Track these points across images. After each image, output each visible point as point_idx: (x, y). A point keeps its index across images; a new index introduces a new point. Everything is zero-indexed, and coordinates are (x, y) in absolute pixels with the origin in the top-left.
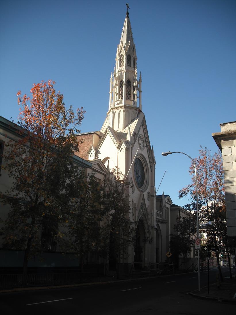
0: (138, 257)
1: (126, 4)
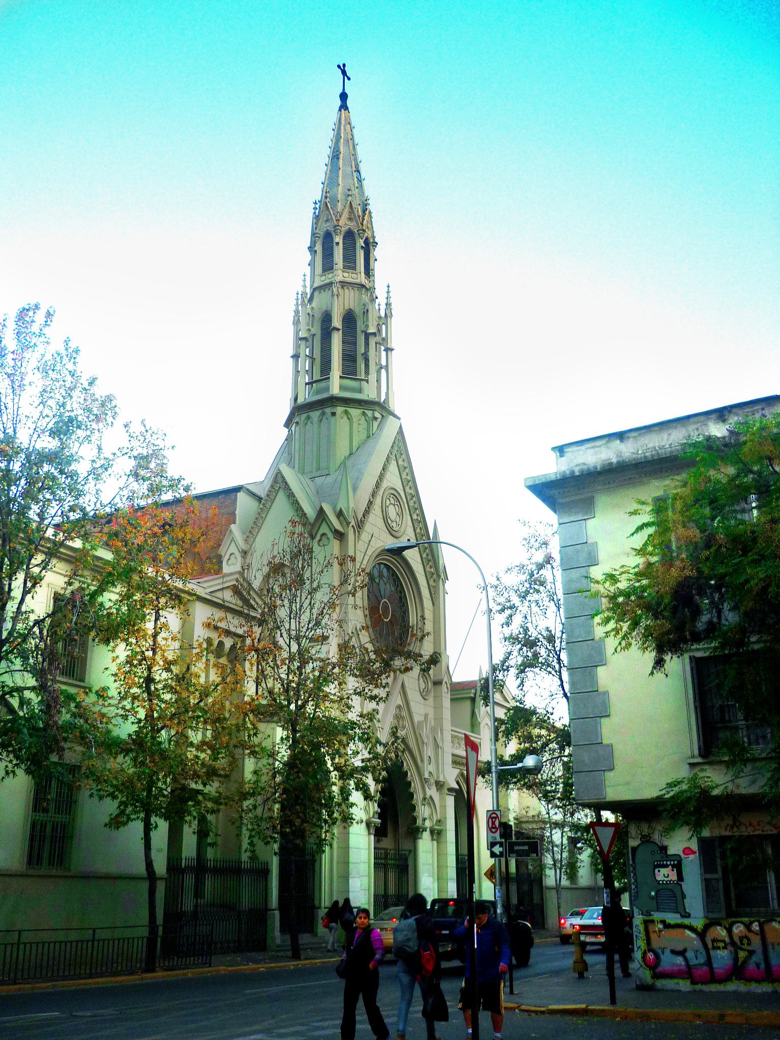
0: (148, 828)
1: (339, 66)
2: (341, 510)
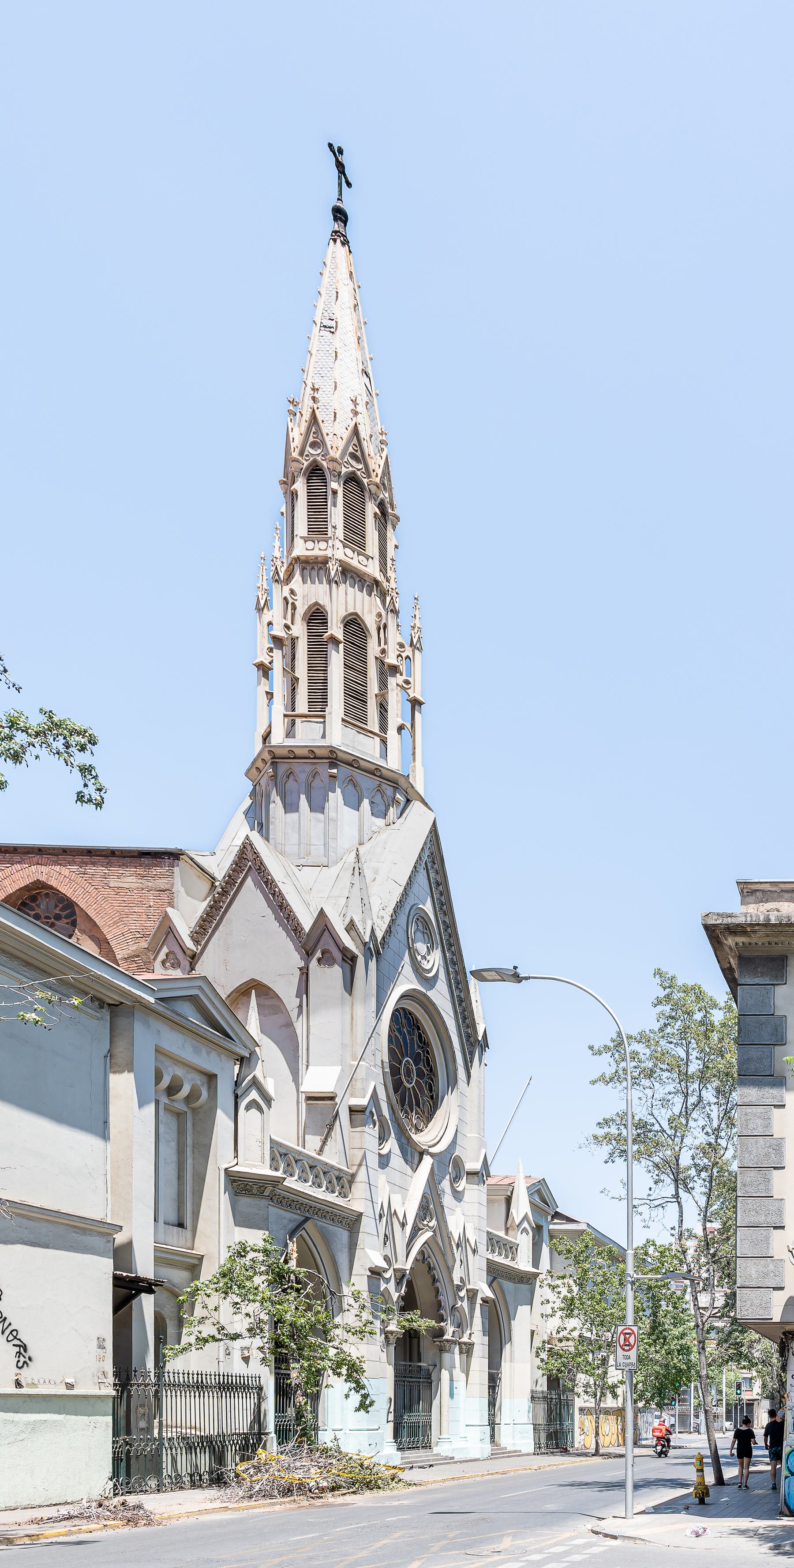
2: (352, 921)
